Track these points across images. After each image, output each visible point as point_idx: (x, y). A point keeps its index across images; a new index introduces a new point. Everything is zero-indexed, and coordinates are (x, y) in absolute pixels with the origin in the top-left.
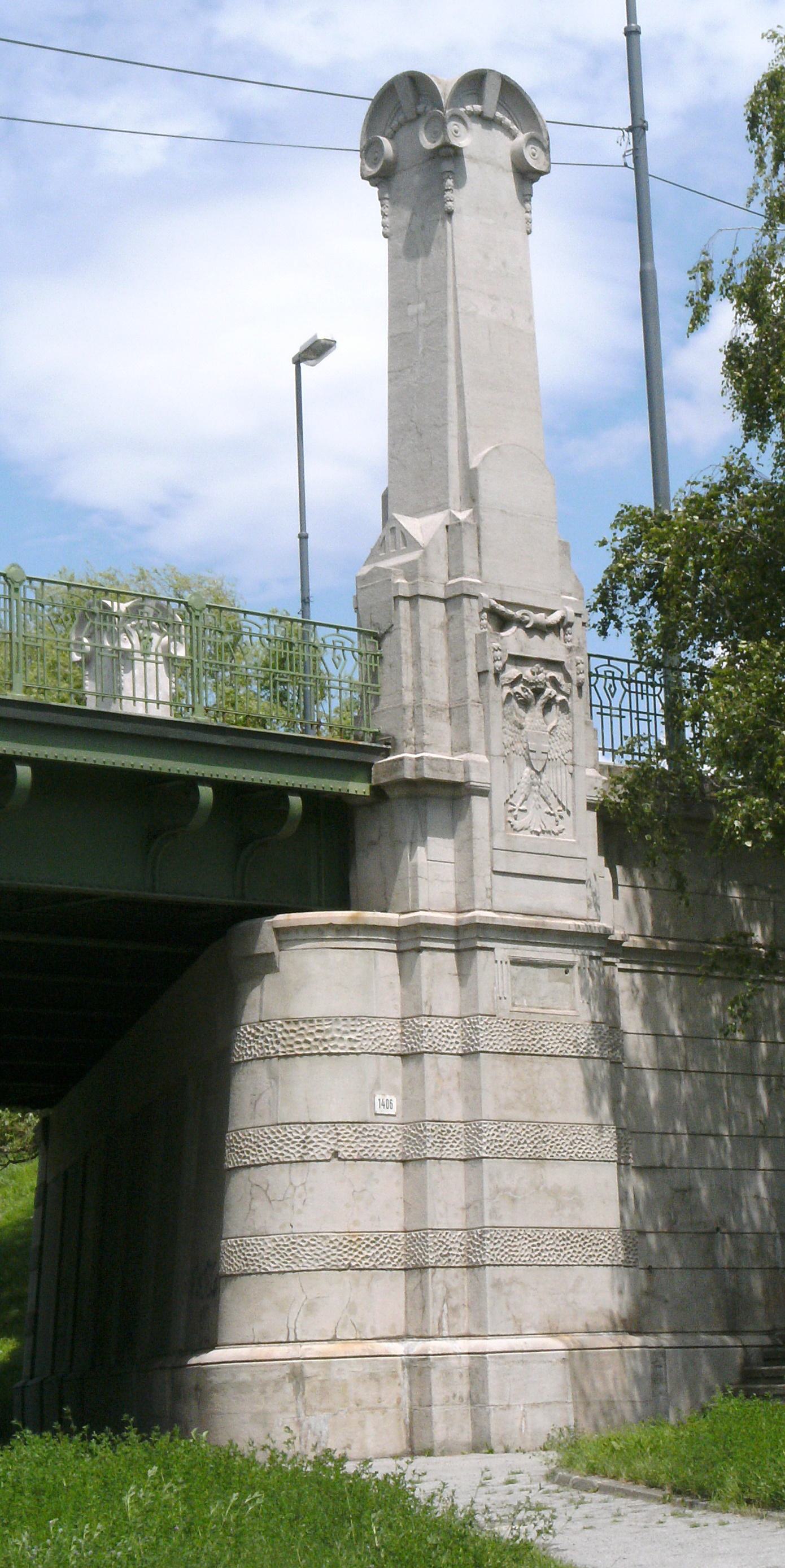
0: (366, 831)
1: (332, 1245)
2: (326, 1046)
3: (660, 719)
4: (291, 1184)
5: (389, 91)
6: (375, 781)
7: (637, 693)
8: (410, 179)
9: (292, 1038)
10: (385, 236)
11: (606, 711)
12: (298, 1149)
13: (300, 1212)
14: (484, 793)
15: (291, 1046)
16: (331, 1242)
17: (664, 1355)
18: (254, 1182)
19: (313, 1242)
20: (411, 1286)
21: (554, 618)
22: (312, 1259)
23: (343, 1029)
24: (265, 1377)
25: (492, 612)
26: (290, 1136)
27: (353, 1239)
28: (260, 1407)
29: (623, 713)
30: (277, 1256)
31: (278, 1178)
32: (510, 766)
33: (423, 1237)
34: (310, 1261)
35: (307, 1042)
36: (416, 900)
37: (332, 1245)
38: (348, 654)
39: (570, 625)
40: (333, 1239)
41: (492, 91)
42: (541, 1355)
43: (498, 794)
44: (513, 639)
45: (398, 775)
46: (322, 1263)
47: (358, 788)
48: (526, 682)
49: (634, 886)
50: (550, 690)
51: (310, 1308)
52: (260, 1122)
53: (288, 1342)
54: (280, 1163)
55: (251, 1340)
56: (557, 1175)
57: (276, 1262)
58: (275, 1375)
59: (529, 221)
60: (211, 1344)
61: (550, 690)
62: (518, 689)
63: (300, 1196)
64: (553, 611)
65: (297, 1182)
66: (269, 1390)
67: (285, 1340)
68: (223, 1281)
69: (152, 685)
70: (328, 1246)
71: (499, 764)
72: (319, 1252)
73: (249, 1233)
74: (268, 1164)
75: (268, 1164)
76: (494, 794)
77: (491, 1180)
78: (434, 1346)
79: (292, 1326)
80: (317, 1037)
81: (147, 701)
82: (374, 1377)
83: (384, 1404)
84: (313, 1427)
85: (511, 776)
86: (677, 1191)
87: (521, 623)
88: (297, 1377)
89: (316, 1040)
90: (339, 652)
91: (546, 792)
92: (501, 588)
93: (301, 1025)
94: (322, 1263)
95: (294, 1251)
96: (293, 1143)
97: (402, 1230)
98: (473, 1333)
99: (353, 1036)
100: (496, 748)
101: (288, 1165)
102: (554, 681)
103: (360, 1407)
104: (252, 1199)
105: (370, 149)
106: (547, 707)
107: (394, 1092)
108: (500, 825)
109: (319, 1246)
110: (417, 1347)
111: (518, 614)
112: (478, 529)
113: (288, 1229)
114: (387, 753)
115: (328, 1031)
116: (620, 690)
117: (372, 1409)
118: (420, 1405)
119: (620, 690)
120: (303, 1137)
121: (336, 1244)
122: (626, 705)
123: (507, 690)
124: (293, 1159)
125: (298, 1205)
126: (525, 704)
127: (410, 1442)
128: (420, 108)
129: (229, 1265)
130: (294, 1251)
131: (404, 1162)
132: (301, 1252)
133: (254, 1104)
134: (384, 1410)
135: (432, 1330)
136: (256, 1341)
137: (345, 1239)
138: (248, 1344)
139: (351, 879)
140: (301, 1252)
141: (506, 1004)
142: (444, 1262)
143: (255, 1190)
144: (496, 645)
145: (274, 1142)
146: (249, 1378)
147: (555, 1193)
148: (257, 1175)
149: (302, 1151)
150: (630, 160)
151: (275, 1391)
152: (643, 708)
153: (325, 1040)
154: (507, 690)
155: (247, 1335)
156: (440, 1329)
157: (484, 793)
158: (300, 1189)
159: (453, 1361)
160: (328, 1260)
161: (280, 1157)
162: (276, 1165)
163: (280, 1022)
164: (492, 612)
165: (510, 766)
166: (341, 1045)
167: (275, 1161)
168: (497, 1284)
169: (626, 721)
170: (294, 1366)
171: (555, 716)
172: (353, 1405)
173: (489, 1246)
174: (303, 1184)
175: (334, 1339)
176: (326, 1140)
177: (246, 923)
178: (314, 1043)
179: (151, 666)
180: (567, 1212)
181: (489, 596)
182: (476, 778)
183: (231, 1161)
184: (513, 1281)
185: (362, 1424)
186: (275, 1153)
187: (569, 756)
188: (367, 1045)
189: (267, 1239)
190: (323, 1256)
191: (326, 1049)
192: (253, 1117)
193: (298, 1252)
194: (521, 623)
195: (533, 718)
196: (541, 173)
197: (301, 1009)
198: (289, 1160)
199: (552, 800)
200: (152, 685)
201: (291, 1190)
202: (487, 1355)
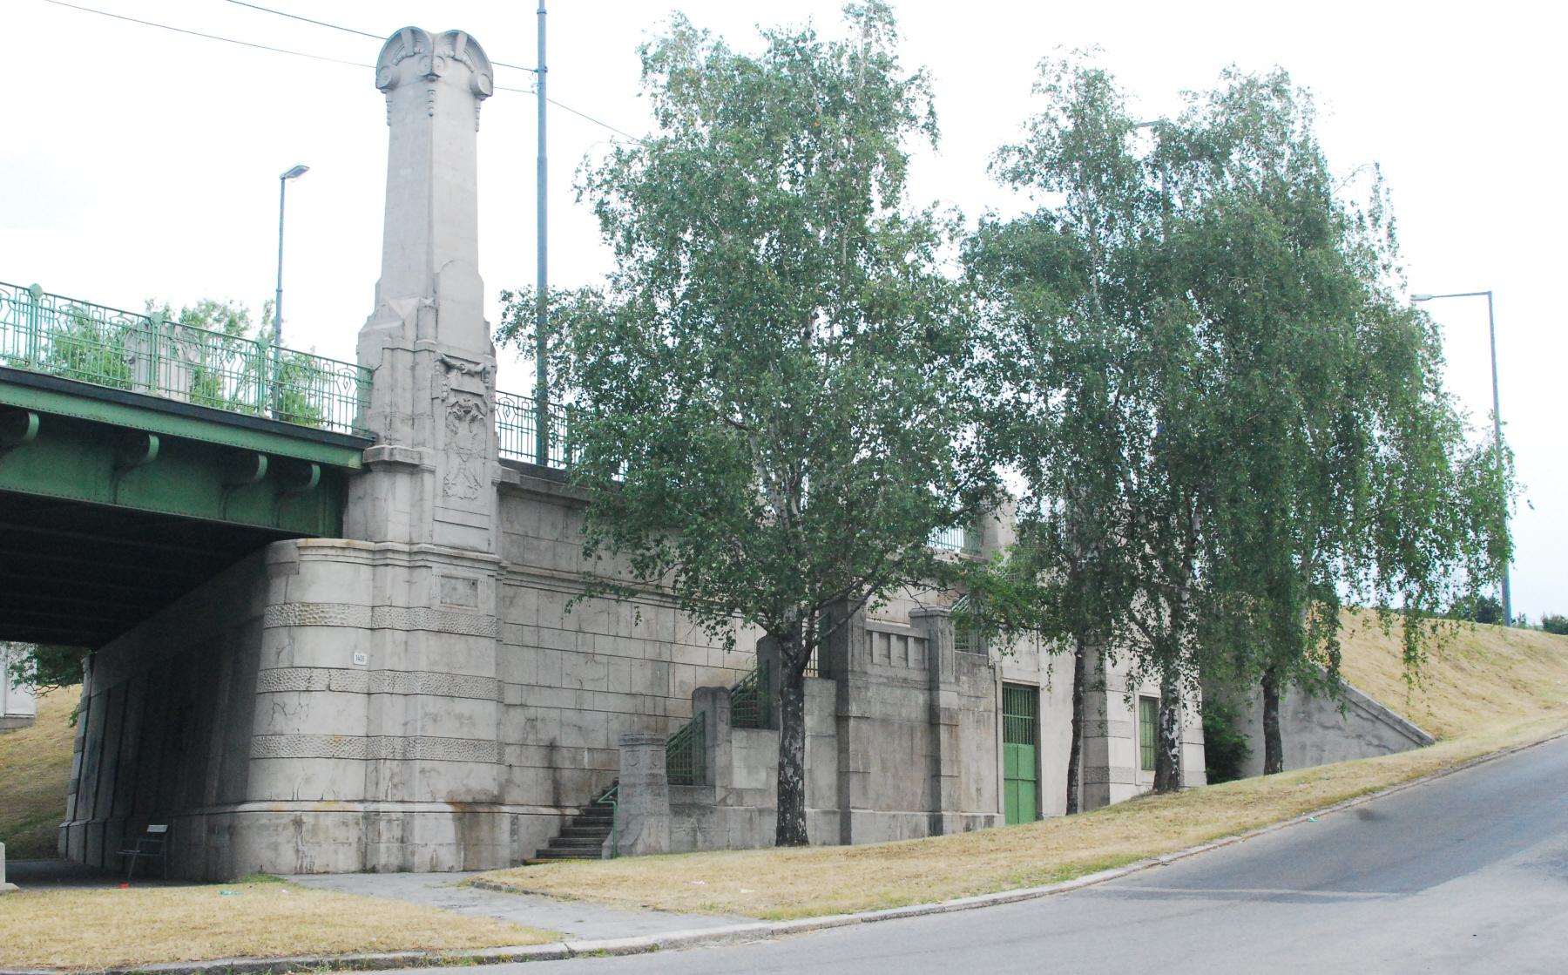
0: (355, 492)
3: (535, 433)
5: (397, 37)
7: (19, 311)
8: (407, 92)
10: (389, 125)
11: (503, 426)
14: (432, 472)
17: (517, 818)
20: (369, 770)
21: (479, 368)
24: (279, 821)
25: (443, 362)
27: (337, 740)
28: (273, 840)
29: (7, 326)
31: (292, 700)
32: (448, 457)
36: (386, 535)
38: (353, 381)
39: (489, 373)
41: (462, 41)
43: (440, 474)
44: (454, 379)
47: (354, 462)
48: (461, 406)
49: (325, 503)
50: (474, 412)
51: (308, 780)
52: (281, 665)
56: (463, 707)
59: (477, 124)
60: (244, 802)
61: (474, 412)
62: (455, 410)
64: (478, 364)
66: (280, 829)
68: (251, 763)
69: (174, 379)
71: (441, 455)
76: (437, 473)
77: (423, 708)
78: (382, 807)
81: (340, 425)
82: (345, 824)
83: (350, 840)
85: (448, 463)
86: (528, 720)
87: (460, 369)
88: (298, 823)
90: (347, 379)
91: (467, 473)
92: (449, 347)
99: (343, 616)
100: (441, 445)
102: (477, 405)
105: (381, 68)
106: (474, 419)
107: (365, 652)
108: (440, 492)
110: (372, 807)
111: (458, 363)
112: (437, 311)
113: (297, 732)
114: (373, 443)
115: (328, 612)
116: (512, 414)
117: (343, 843)
119: (512, 414)
122: (515, 423)
123: (449, 410)
125: (303, 717)
126: (459, 418)
127: (365, 866)
128: (416, 50)
129: (254, 753)
131: (369, 694)
133: (278, 654)
134: (350, 844)
135: (382, 797)
139: (345, 519)
141: (437, 602)
142: (391, 756)
143: (277, 708)
144: (444, 382)
147: (460, 717)
148: (278, 698)
150: (536, 89)
152: (525, 425)
154: (449, 410)
155: (267, 795)
156: (386, 796)
157: (432, 472)
158: (305, 707)
159: (394, 816)
164: (443, 362)
165: (448, 457)
168: (423, 771)
169: (514, 433)
170: (296, 816)
171: (475, 427)
173: (419, 747)
175: (322, 800)
177: (277, 543)
179: (350, 405)
180: (466, 729)
181: (441, 352)
182: (427, 462)
183: (261, 688)
184: (433, 770)
185: (336, 852)
187: (483, 453)
188: (351, 622)
189: (282, 738)
192: (277, 663)
194: (460, 369)
195: (463, 428)
196: (487, 96)
197: (312, 596)
199: (472, 479)
200: (174, 379)
201: (299, 708)
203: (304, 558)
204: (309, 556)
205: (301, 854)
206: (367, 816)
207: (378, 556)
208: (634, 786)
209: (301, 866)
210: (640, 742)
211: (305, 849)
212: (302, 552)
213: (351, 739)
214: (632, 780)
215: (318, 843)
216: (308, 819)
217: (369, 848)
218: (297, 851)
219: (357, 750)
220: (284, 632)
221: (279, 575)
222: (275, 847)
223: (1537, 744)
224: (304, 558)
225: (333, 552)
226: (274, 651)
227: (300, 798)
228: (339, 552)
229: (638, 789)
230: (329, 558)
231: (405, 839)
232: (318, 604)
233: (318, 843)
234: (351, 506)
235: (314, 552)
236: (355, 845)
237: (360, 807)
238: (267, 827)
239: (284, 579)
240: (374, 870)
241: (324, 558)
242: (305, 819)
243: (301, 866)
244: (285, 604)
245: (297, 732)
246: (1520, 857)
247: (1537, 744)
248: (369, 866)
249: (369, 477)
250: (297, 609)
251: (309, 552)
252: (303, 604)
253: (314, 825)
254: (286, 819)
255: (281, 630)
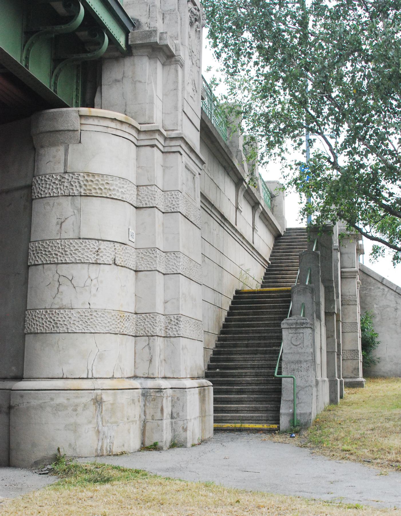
1: (112, 318)
2: (111, 193)
4: (89, 277)
6: (131, 42)
9: (90, 185)
12: (94, 255)
13: (95, 295)
15: (90, 190)
16: (112, 316)
18: (61, 274)
19: (102, 315)
22: (102, 326)
23: (119, 185)
24: (77, 401)
26: (88, 246)
28: (72, 420)
30: (81, 322)
33: (153, 318)
34: (101, 327)
35: (101, 189)
37: (112, 318)
40: (113, 314)
42: (51, 393)
45: (152, 40)
46: (107, 329)
51: (101, 357)
53: (87, 378)
54: (82, 263)
55: (61, 376)
57: (80, 326)
58: (84, 400)
60: (20, 378)
63: (95, 285)
65: (93, 276)
66: (80, 409)
67: (86, 377)
70: (111, 319)
72: (106, 322)
73: (57, 307)
74: (73, 263)
75: (73, 263)
79: (90, 368)
80: (106, 187)
84: (106, 434)
88: (98, 402)
89: (105, 188)
93: (97, 178)
94: (107, 329)
95: (91, 320)
96: (91, 251)
97: (134, 312)
98: (168, 376)
101: (87, 265)
103: (129, 420)
104: (60, 285)
109: (106, 318)
110: (150, 384)
115: (112, 185)
118: (153, 419)
120: (97, 249)
121: (115, 318)
124: (91, 262)
125: (94, 291)
127: (143, 443)
130: (91, 320)
132: (96, 321)
136: (65, 377)
137: (118, 315)
138: (58, 378)
140: (96, 321)
143: (62, 279)
145: (78, 249)
146: (66, 401)
148: (63, 270)
149: (96, 257)
151: (83, 410)
153: (110, 189)
158: (94, 282)
160: (111, 328)
161: (82, 260)
162: (79, 265)
163: (82, 174)
166: (118, 194)
167: (78, 261)
172: (126, 419)
174: (97, 278)
175: (113, 378)
176: (110, 252)
178: (104, 191)
186: (78, 257)
190: (108, 324)
191: (110, 195)
192: (60, 232)
193: (94, 321)
197: (95, 167)
198: (88, 262)
201: (89, 281)
202: (187, 390)
203: (84, 128)
204: (91, 125)
205: (101, 436)
206: (146, 394)
207: (142, 136)
208: (299, 362)
209: (102, 447)
210: (304, 326)
211: (106, 429)
212: (83, 122)
213: (121, 315)
214: (297, 358)
215: (116, 422)
216: (107, 397)
217: (148, 425)
218: (98, 432)
219: (130, 327)
220: (66, 202)
221: (54, 144)
222: (74, 428)
223: (193, 339)
224: (84, 128)
225: (113, 125)
226: (54, 221)
227: (95, 376)
228: (118, 126)
229: (304, 365)
230: (109, 130)
231: (175, 415)
232: (103, 175)
233: (116, 422)
234: (104, 88)
235: (96, 122)
236: (138, 422)
237: (136, 383)
238: (59, 408)
239: (62, 149)
240: (155, 447)
241: (105, 129)
242: (105, 397)
243: (102, 447)
244: (66, 172)
245: (88, 306)
246: (208, 379)
247: (193, 339)
248: (148, 443)
249: (128, 62)
250: (81, 178)
251: (90, 121)
252: (88, 174)
253: (112, 404)
254: (86, 398)
255: (62, 200)
